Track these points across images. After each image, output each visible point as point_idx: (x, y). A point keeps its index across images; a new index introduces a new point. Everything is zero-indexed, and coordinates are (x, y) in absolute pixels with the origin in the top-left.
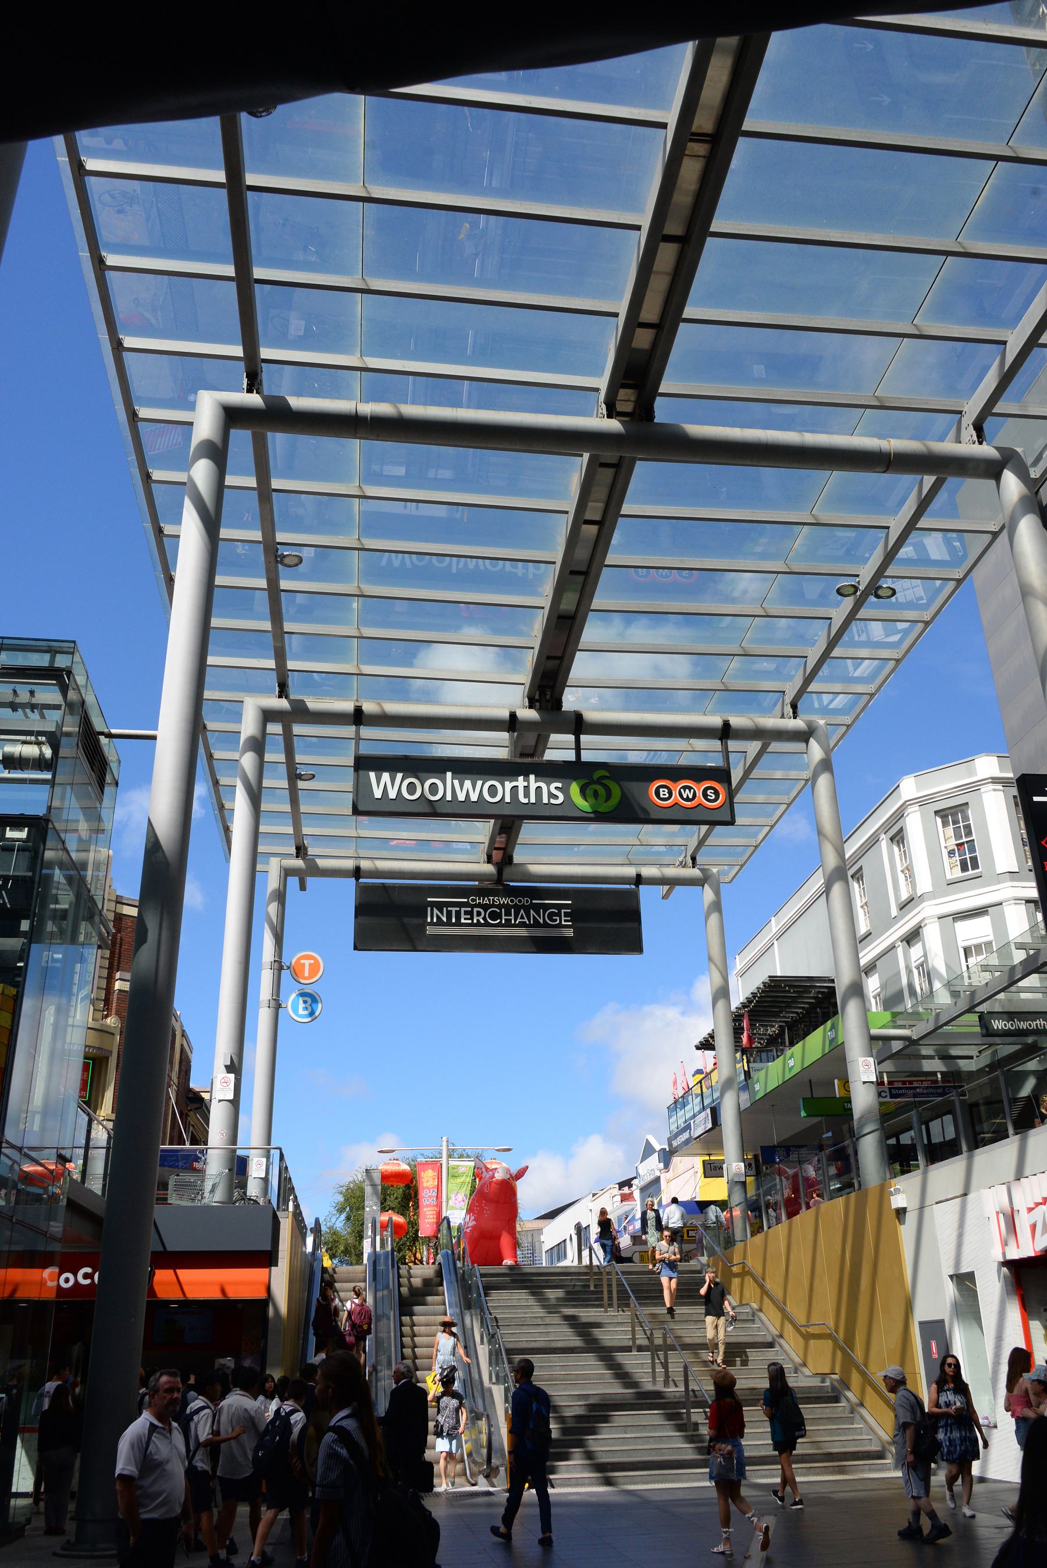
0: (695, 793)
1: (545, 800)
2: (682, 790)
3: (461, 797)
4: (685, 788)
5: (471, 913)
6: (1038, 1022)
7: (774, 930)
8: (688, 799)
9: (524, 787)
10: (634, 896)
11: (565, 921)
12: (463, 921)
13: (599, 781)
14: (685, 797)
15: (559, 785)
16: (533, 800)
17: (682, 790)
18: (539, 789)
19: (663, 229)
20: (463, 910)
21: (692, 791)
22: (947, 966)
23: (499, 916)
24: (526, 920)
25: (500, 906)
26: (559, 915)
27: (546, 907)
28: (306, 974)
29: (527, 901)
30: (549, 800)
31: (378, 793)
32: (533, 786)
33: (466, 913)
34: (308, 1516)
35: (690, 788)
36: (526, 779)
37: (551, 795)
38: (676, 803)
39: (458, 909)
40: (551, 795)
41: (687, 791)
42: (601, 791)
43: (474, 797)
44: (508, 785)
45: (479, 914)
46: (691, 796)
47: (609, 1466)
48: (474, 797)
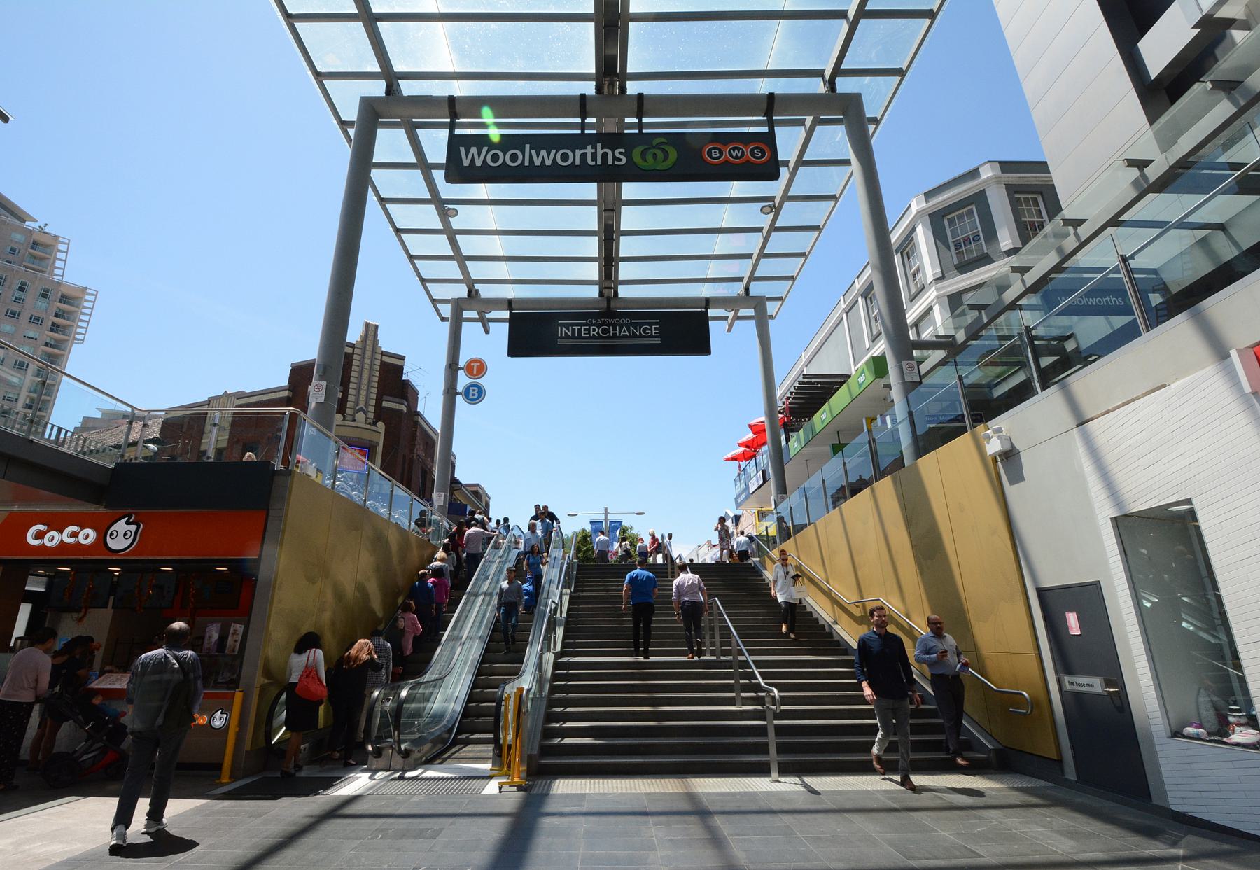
1: (610, 162)
2: (732, 151)
3: (538, 163)
4: (734, 149)
5: (589, 330)
6: (1108, 298)
7: (804, 360)
8: (737, 157)
9: (592, 153)
11: (655, 333)
12: (583, 335)
13: (658, 146)
14: (734, 155)
15: (623, 151)
16: (599, 162)
17: (732, 151)
18: (605, 156)
20: (583, 328)
21: (741, 151)
24: (627, 333)
25: (609, 325)
26: (651, 329)
27: (641, 325)
28: (475, 372)
30: (613, 162)
31: (466, 162)
32: (600, 152)
35: (739, 149)
36: (594, 147)
37: (615, 158)
38: (725, 145)
39: (579, 327)
40: (615, 158)
41: (736, 151)
42: (660, 154)
43: (548, 163)
44: (578, 153)
45: (594, 330)
46: (739, 155)
47: (1228, 167)
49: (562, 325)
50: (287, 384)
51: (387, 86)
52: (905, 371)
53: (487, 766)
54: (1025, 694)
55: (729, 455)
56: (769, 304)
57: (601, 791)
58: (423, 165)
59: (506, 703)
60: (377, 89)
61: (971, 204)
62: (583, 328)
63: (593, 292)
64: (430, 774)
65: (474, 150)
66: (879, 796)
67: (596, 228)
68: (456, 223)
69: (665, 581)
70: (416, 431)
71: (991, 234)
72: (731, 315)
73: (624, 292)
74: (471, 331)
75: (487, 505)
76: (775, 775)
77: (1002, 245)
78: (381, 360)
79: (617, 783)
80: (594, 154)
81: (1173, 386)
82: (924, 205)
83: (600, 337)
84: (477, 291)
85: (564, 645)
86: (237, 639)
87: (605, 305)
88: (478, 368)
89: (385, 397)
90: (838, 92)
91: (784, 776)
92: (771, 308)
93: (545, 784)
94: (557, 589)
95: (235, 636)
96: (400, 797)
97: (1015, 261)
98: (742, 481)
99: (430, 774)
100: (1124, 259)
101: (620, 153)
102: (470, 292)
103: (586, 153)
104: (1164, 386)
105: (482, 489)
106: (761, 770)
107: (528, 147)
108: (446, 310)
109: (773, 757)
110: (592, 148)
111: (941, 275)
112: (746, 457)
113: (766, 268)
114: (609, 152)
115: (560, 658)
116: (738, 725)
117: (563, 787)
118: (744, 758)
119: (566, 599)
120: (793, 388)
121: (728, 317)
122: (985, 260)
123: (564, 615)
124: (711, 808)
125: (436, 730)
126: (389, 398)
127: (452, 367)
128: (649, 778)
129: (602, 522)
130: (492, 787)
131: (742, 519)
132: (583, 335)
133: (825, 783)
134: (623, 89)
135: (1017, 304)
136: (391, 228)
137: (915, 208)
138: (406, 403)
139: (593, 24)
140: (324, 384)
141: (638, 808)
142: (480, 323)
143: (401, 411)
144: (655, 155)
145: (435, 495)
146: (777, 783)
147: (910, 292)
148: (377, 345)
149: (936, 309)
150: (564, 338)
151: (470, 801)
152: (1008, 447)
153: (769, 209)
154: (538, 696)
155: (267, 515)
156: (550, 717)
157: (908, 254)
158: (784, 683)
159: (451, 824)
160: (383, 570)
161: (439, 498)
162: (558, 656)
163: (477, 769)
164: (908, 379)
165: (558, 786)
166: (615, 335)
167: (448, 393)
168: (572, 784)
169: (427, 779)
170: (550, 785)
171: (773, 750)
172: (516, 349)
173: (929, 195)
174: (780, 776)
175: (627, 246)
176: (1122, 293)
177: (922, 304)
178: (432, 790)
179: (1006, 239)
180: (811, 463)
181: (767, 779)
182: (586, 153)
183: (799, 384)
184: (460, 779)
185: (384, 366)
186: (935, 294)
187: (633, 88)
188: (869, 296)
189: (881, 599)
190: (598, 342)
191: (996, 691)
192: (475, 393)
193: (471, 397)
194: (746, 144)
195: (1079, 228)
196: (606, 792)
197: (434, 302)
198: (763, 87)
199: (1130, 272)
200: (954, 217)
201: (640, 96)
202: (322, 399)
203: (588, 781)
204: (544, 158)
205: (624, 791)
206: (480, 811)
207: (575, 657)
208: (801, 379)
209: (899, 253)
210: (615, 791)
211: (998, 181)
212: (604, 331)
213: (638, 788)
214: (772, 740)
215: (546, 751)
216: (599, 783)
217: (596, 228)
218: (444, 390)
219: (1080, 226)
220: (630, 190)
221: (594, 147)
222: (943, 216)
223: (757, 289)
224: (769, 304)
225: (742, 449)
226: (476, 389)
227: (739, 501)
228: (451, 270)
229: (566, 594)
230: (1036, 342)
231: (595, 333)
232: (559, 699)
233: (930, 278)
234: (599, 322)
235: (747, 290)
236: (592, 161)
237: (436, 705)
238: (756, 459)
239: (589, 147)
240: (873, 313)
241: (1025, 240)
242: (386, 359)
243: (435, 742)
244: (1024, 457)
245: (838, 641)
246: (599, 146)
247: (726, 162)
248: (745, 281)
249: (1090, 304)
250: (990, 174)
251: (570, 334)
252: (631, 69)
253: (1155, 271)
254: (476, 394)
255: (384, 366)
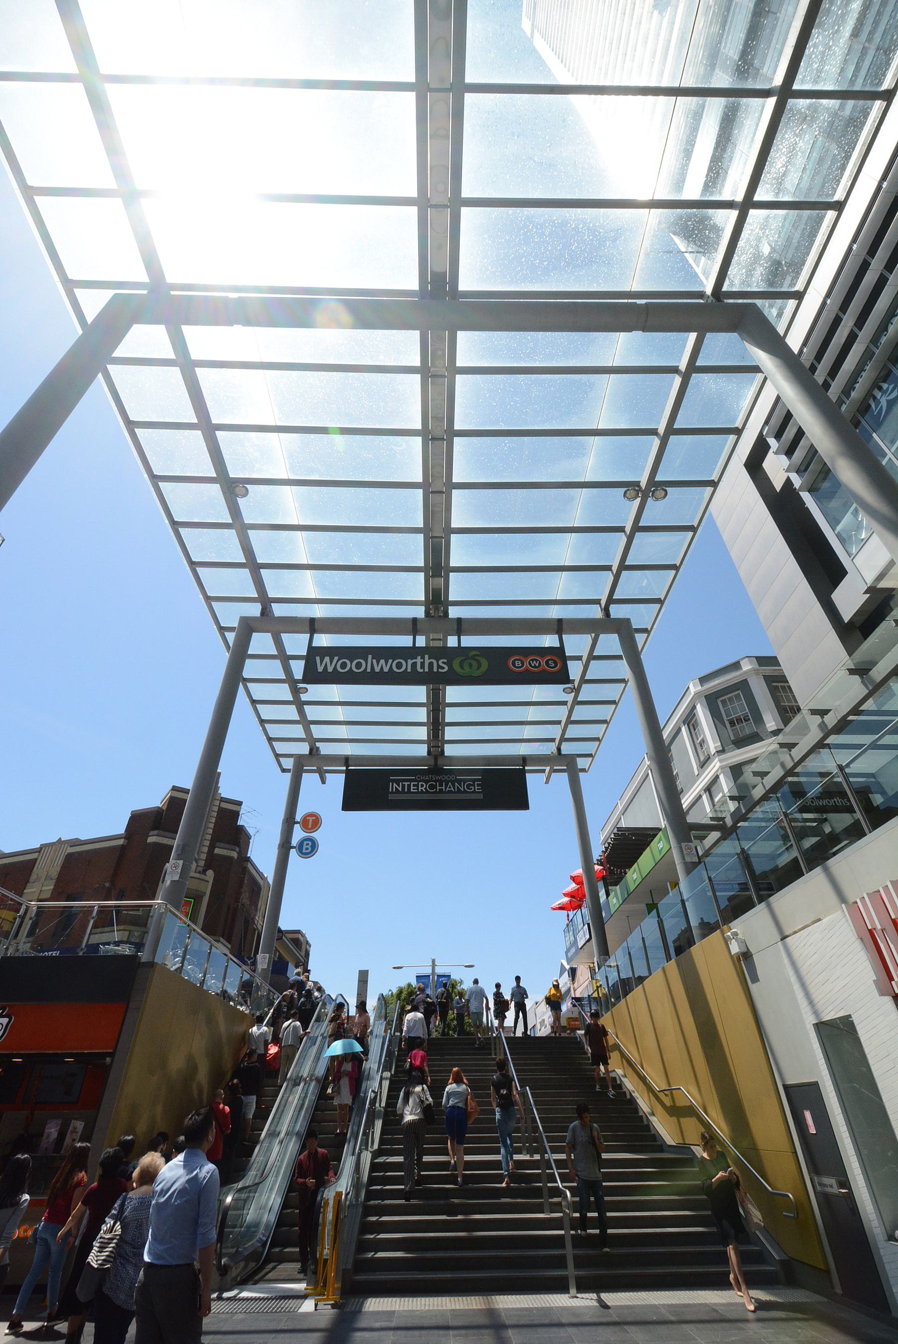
0: (540, 663)
1: (435, 670)
3: (377, 669)
4: (533, 660)
5: (417, 786)
7: (620, 808)
10: (522, 774)
12: (412, 790)
13: (473, 658)
14: (533, 665)
15: (446, 661)
16: (427, 670)
18: (431, 664)
19: (683, 1117)
20: (412, 783)
21: (538, 662)
22: (740, 827)
23: (434, 787)
24: (452, 789)
27: (465, 781)
28: (310, 826)
29: (453, 778)
30: (438, 670)
31: (320, 669)
33: (414, 785)
34: (459, 1179)
35: (536, 660)
36: (423, 658)
37: (439, 667)
40: (439, 667)
41: (535, 662)
42: (474, 664)
44: (410, 662)
45: (422, 786)
46: (537, 665)
48: (386, 669)
49: (393, 781)
50: (123, 832)
51: (262, 609)
52: (685, 852)
53: (301, 1286)
54: (791, 1196)
55: (556, 904)
56: (579, 760)
57: (410, 1309)
58: (285, 658)
59: (324, 1210)
60: (254, 610)
61: (738, 689)
62: (412, 783)
63: (422, 751)
64: (245, 1294)
65: (327, 659)
66: (663, 1310)
67: (425, 701)
68: (304, 697)
69: (485, 1060)
70: (244, 878)
71: (758, 719)
72: (548, 769)
73: (450, 750)
74: (309, 780)
75: (307, 954)
76: (573, 1291)
77: (767, 726)
78: (219, 806)
79: (425, 1301)
80: (423, 664)
81: (824, 921)
82: (699, 688)
83: (427, 792)
84: (318, 748)
85: (382, 1141)
86: (75, 1138)
87: (432, 762)
88: (313, 822)
89: (218, 844)
90: (611, 617)
91: (581, 1293)
92: (581, 763)
93: (358, 1303)
94: (378, 1071)
95: (74, 1134)
96: (223, 1316)
97: (780, 738)
98: (571, 933)
99: (245, 1294)
100: (841, 768)
101: (443, 663)
102: (311, 750)
103: (416, 662)
104: (819, 920)
105: (303, 935)
106: (560, 1287)
107: (370, 657)
108: (288, 763)
109: (571, 1272)
110: (421, 659)
111: (721, 749)
112: (573, 906)
113: (573, 731)
114: (435, 662)
115: (376, 1159)
116: (545, 1235)
117: (374, 1305)
118: (548, 1272)
119: (386, 1084)
120: (610, 839)
121: (555, 739)
122: (755, 738)
123: (383, 1104)
124: (507, 1322)
125: (251, 1244)
126: (222, 845)
127: (289, 821)
128: (456, 1296)
129: (429, 976)
130: (308, 1306)
131: (578, 973)
132: (412, 790)
133: (615, 1299)
134: (446, 613)
135: (825, 742)
136: (248, 700)
137: (693, 690)
138: (237, 849)
139: (423, 573)
140: (181, 862)
141: (441, 1323)
142: (318, 774)
143: (230, 859)
144: (470, 665)
145: (259, 956)
146: (575, 1299)
147: (699, 759)
148: (217, 791)
149: (722, 777)
150: (394, 793)
151: (288, 1318)
152: (745, 950)
153: (570, 691)
154: (354, 1203)
155: (128, 1005)
156: (367, 1228)
157: (693, 725)
158: (615, 1186)
159: (273, 1338)
160: (214, 1053)
161: (263, 961)
162: (376, 1154)
163: (291, 1290)
164: (688, 859)
165: (370, 1304)
166: (441, 790)
167: (283, 847)
168: (383, 1302)
169: (245, 1300)
170: (362, 1303)
171: (570, 1263)
172: (352, 802)
173: (703, 680)
174: (577, 1293)
175: (450, 715)
176: (843, 795)
177: (707, 776)
178: (252, 1309)
179: (771, 722)
180: (631, 922)
181: (567, 1295)
182: (416, 662)
183: (615, 836)
184: (272, 1299)
185: (221, 811)
186: (718, 765)
187: (454, 612)
188: (691, 723)
189: (681, 1088)
190: (426, 797)
191: (771, 1193)
192: (309, 847)
193: (304, 851)
194: (542, 656)
195: (825, 716)
196: (414, 1309)
197: (277, 756)
198: (554, 612)
199: (846, 776)
200: (725, 699)
201: (459, 620)
202: (176, 878)
203: (398, 1299)
204: (383, 666)
205: (431, 1308)
206: (298, 1327)
207: (392, 1156)
208: (615, 831)
209: (686, 725)
210: (423, 1308)
211: (757, 673)
212: (432, 787)
213: (444, 1305)
214: (569, 1251)
215: (362, 1266)
216: (409, 1301)
217: (425, 701)
218: (279, 845)
219: (826, 715)
220: (453, 693)
221: (423, 658)
222: (717, 698)
223: (567, 749)
224: (579, 760)
225: (566, 899)
226: (310, 843)
227: (569, 955)
228: (298, 731)
229: (386, 1079)
230: (851, 779)
231: (423, 788)
232: (375, 1206)
233: (713, 751)
234: (427, 778)
235: (559, 749)
236: (421, 669)
237: (251, 1215)
238: (581, 910)
239: (419, 658)
240: (698, 739)
241: (786, 721)
242: (224, 805)
243: (248, 1259)
244: (755, 958)
245: (654, 1135)
246: (427, 657)
247: (527, 670)
248: (557, 741)
249: (821, 804)
250: (749, 667)
251: (400, 789)
252: (451, 598)
253: (872, 775)
254: (309, 848)
255: (221, 811)
